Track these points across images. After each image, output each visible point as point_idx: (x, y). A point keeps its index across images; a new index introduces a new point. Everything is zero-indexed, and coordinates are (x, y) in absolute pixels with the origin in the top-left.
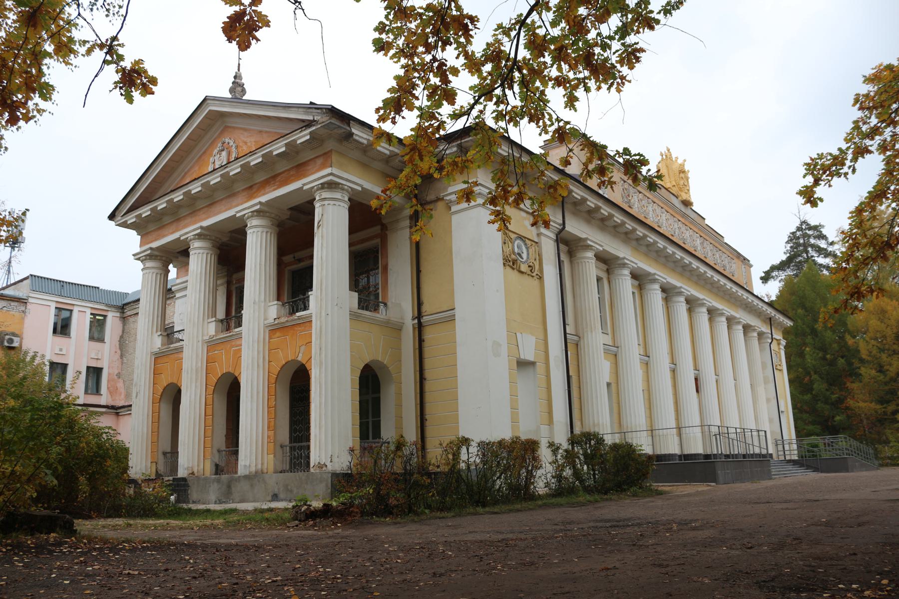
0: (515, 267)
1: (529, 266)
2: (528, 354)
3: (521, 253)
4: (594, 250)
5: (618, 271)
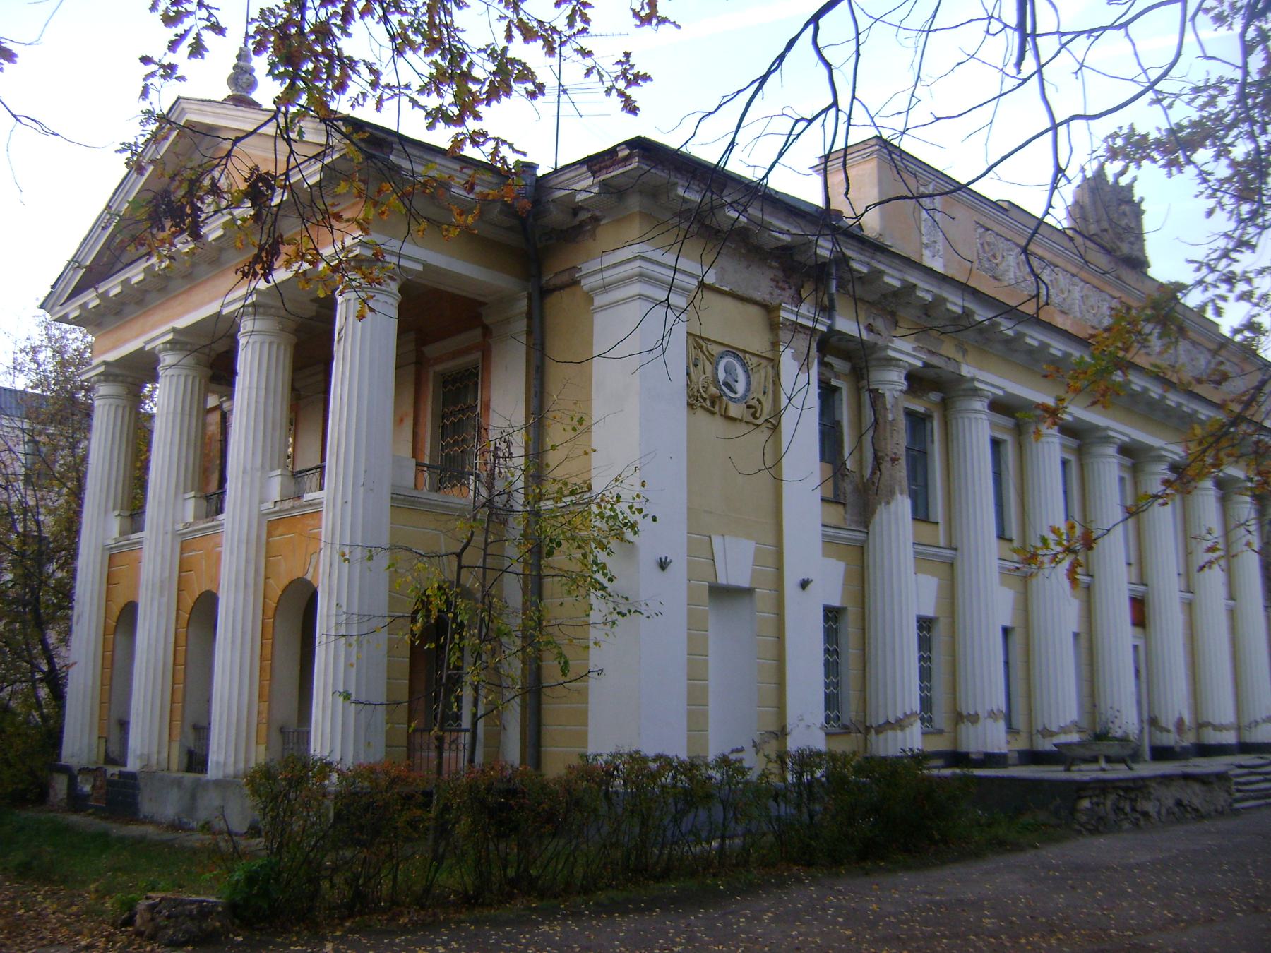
0: (717, 409)
1: (749, 407)
3: (730, 381)
4: (903, 367)
5: (962, 404)
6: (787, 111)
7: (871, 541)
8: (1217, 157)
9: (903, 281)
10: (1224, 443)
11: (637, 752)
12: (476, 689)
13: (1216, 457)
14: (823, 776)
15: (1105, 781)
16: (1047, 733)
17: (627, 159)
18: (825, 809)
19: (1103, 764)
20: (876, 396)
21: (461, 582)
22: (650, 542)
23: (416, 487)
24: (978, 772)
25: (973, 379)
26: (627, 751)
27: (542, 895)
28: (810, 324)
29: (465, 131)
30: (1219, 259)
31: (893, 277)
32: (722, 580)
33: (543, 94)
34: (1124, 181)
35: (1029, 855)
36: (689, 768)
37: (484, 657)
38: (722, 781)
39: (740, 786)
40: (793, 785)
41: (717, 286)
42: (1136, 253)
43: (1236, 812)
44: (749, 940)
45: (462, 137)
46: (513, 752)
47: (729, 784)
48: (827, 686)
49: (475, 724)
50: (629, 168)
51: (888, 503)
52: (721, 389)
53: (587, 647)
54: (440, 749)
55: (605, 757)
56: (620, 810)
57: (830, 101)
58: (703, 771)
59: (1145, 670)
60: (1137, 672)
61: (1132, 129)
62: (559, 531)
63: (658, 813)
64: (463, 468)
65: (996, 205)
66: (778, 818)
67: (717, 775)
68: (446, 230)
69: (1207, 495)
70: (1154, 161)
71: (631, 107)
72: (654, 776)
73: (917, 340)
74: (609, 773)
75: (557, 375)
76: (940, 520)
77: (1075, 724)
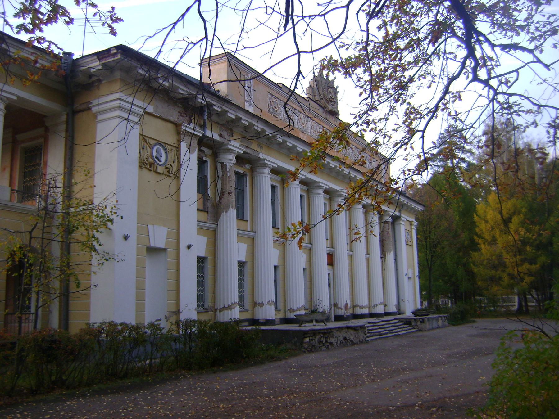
0: (152, 168)
2: (159, 241)
3: (159, 156)
6: (185, 39)
7: (314, 247)
8: (364, 72)
9: (236, 116)
10: (363, 190)
11: (112, 322)
12: (38, 293)
13: (360, 195)
14: (196, 331)
15: (315, 330)
16: (291, 310)
17: (115, 54)
18: (196, 345)
19: (314, 323)
20: (223, 165)
21: (32, 245)
22: (118, 228)
23: (11, 201)
24: (262, 328)
25: (264, 159)
26: (108, 321)
27: (68, 388)
28: (191, 131)
29: (35, 37)
30: (364, 114)
31: (231, 114)
32: (152, 245)
33: (73, 24)
34: (331, 78)
35: (283, 362)
36: (136, 328)
37: (42, 280)
38: (151, 334)
39: (159, 336)
40: (183, 335)
41: (154, 114)
42: (336, 110)
43: (367, 342)
44: (162, 404)
45: (33, 39)
46: (55, 323)
47: (154, 335)
48: (198, 291)
49: (37, 310)
50: (116, 58)
51: (226, 212)
52: (154, 160)
53: (90, 274)
54: (20, 322)
55: (98, 324)
56: (104, 348)
57: (204, 36)
58: (143, 329)
59: (332, 284)
60: (329, 285)
61: (331, 57)
62: (77, 222)
63: (122, 349)
64: (34, 192)
65: (277, 85)
66: (176, 349)
67: (148, 331)
68: (25, 82)
69: (359, 211)
70: (339, 71)
71: (113, 32)
72: (120, 332)
73: (241, 142)
74: (99, 331)
75: (79, 151)
76: (249, 220)
77: (303, 306)
